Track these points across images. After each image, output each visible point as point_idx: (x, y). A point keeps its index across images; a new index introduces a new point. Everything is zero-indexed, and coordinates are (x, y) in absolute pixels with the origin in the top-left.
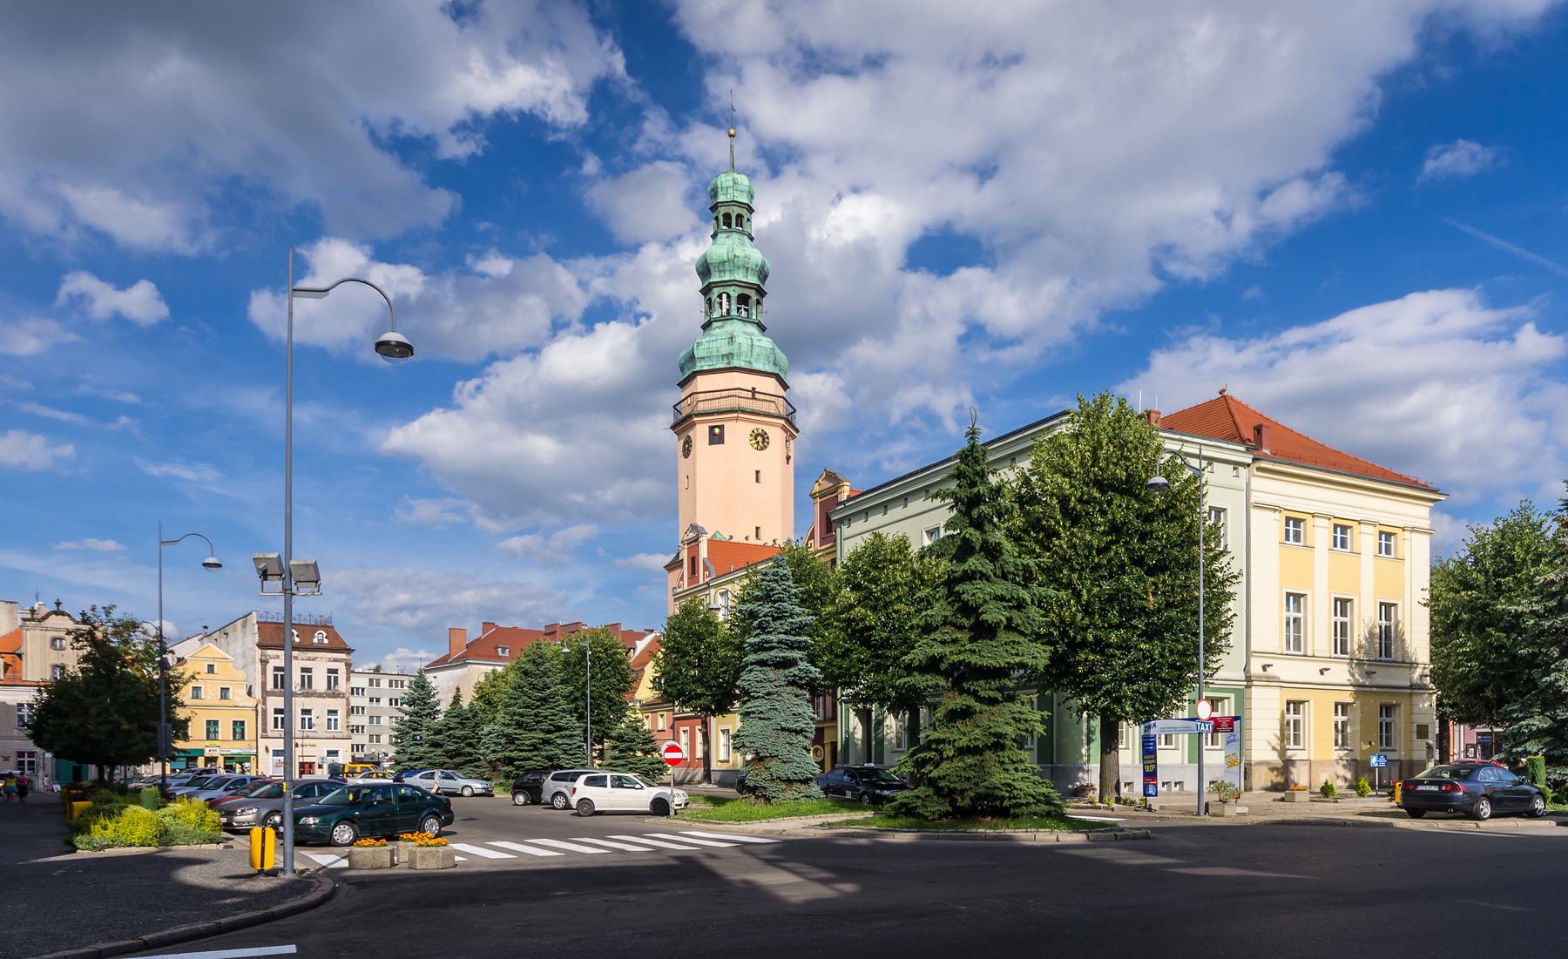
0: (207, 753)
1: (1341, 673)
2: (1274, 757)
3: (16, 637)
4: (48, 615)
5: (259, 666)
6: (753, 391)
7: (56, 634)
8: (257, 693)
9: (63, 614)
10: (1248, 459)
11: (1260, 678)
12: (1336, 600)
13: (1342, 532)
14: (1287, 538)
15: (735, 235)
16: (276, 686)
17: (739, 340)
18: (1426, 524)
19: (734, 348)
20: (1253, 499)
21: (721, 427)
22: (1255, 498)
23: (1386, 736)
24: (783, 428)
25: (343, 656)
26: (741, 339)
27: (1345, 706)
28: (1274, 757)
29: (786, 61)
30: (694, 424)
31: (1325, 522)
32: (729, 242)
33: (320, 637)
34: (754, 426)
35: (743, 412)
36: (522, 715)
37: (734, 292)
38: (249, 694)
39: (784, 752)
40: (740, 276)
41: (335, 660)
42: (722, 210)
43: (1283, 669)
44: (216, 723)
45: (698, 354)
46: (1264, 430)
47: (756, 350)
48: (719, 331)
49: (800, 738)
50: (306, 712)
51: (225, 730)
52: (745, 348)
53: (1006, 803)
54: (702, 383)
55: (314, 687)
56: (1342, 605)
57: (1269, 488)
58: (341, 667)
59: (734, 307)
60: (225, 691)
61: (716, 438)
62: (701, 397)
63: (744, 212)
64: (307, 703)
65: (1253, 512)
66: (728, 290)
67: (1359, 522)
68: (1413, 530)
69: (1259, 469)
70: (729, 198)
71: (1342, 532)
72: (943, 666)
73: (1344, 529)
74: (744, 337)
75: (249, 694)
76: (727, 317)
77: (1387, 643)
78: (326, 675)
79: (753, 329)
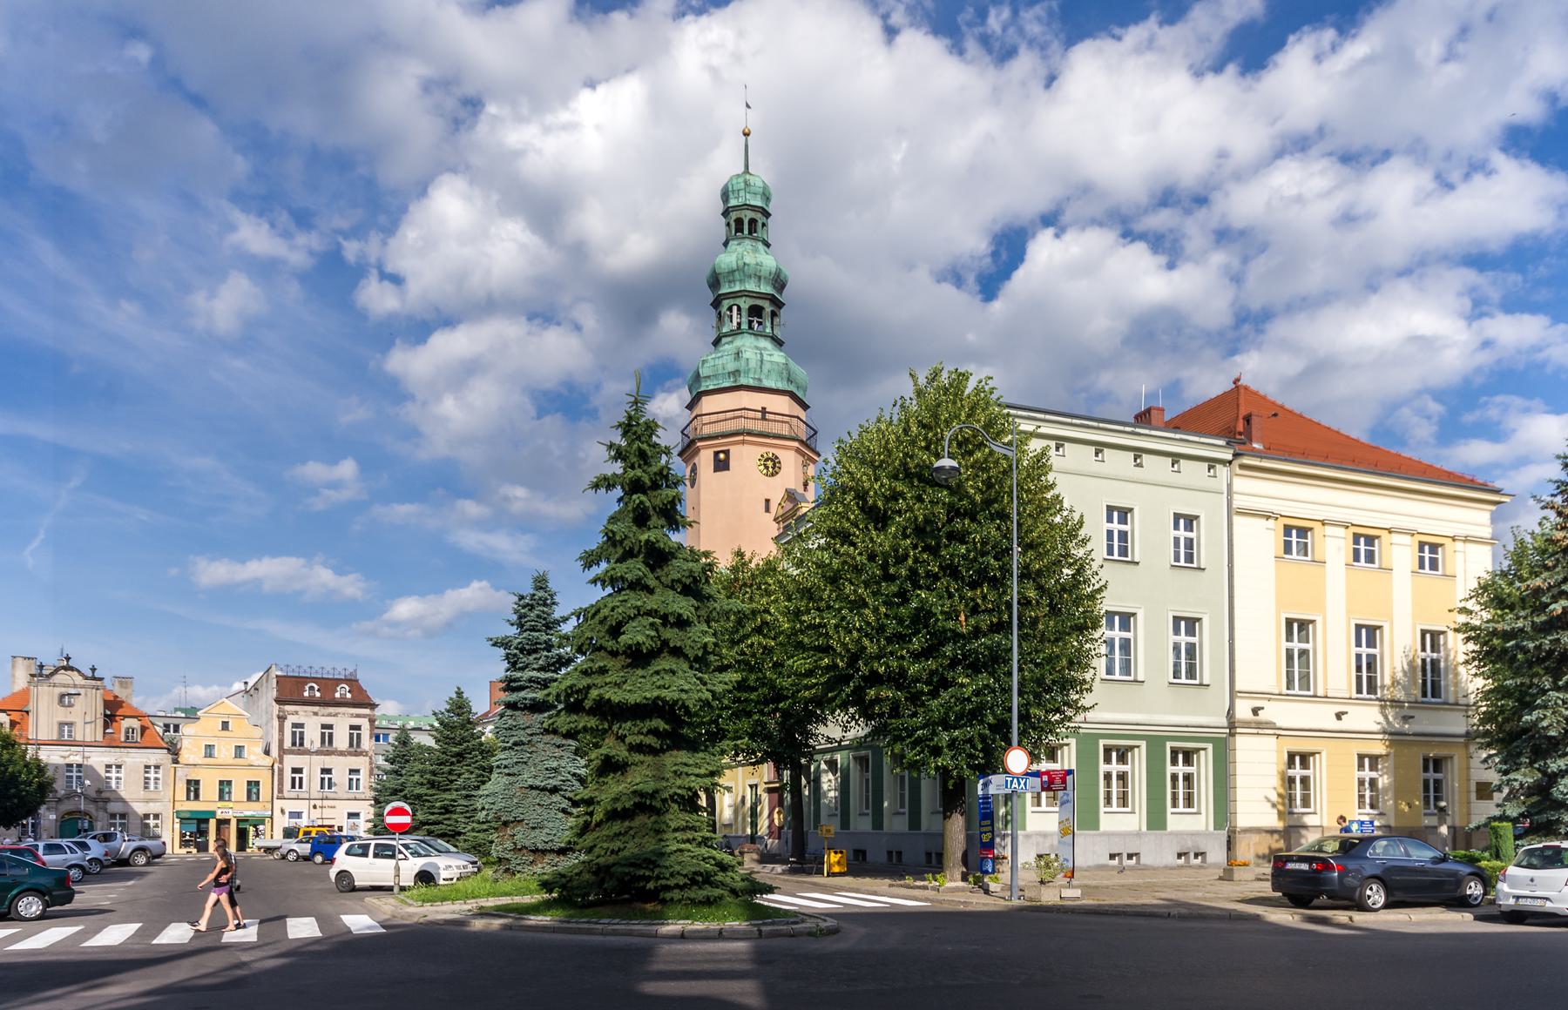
0: (219, 816)
1: (1367, 717)
2: (1272, 820)
3: (25, 694)
4: (56, 671)
5: (276, 723)
6: (764, 411)
7: (64, 690)
8: (275, 751)
9: (72, 669)
10: (1227, 455)
11: (1247, 724)
12: (1359, 627)
13: (1365, 545)
14: (1357, 559)
15: (747, 242)
16: (294, 744)
17: (746, 355)
18: (1486, 532)
19: (742, 365)
20: (1236, 504)
21: (727, 453)
22: (1238, 502)
23: (1434, 792)
24: (798, 450)
25: (367, 711)
26: (749, 354)
27: (1374, 760)
28: (1272, 820)
29: (1219, 166)
30: (698, 450)
31: (1406, 539)
32: (740, 249)
33: (343, 691)
34: (763, 450)
35: (750, 433)
36: (434, 773)
37: (745, 304)
38: (267, 752)
39: (532, 817)
40: (751, 286)
41: (358, 716)
42: (734, 215)
43: (1280, 713)
44: (229, 783)
45: (704, 372)
46: (1255, 421)
47: (767, 367)
48: (728, 347)
49: (556, 798)
50: (296, 770)
51: (239, 791)
52: (753, 364)
53: (651, 885)
54: (708, 404)
55: (335, 744)
56: (1368, 633)
57: (1253, 489)
58: (365, 723)
59: (745, 320)
60: (239, 750)
61: (722, 465)
62: (706, 419)
63: (758, 216)
64: (328, 761)
65: (1237, 519)
66: (738, 301)
67: (1390, 531)
68: (1466, 540)
69: (1242, 467)
70: (741, 201)
71: (1365, 545)
72: (588, 704)
73: (1434, 548)
74: (754, 351)
75: (267, 752)
76: (738, 332)
77: (1431, 680)
78: (319, 730)
79: (765, 344)
